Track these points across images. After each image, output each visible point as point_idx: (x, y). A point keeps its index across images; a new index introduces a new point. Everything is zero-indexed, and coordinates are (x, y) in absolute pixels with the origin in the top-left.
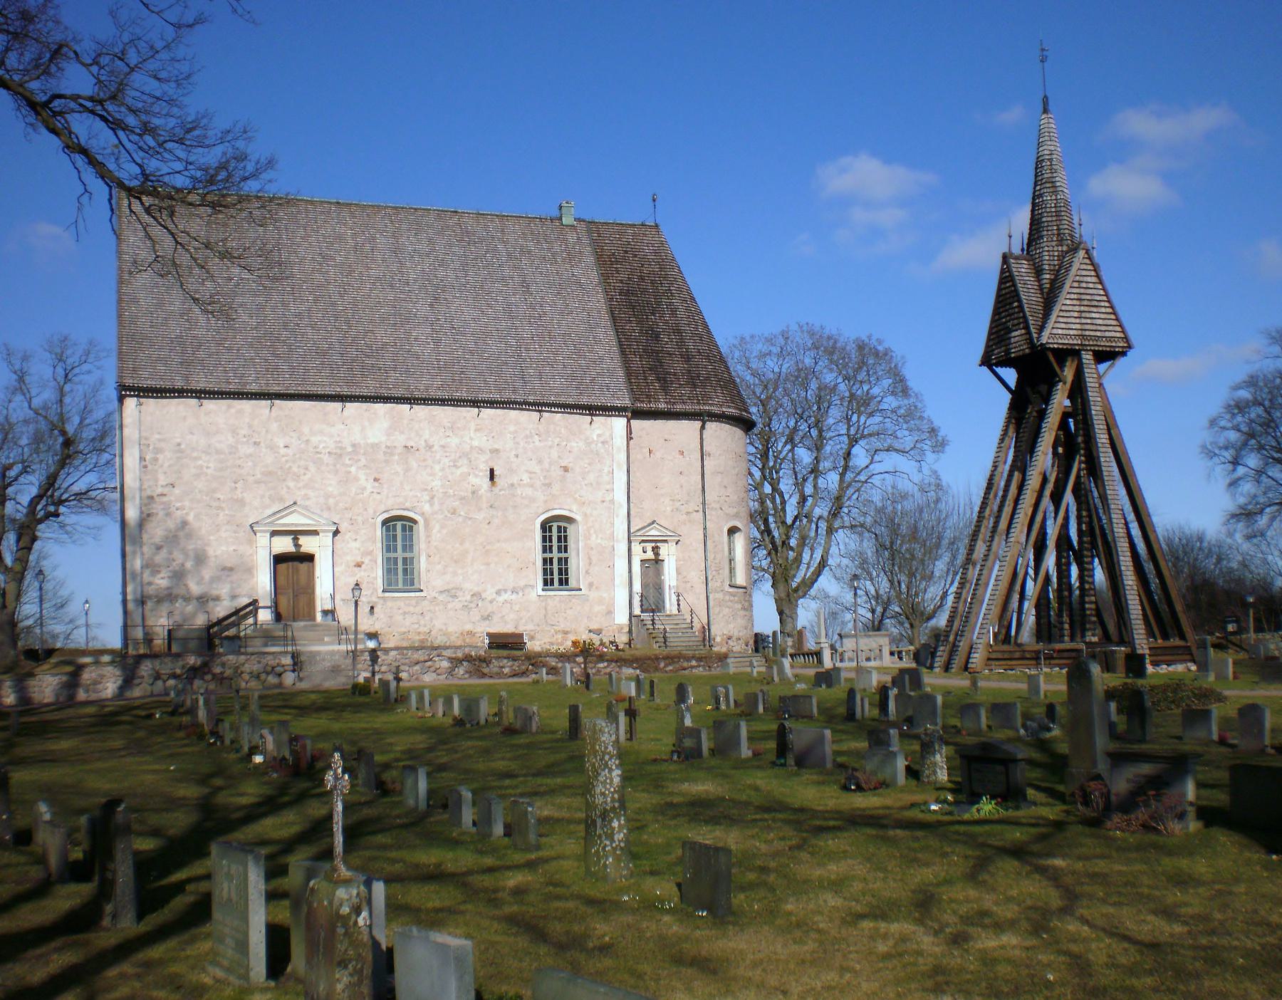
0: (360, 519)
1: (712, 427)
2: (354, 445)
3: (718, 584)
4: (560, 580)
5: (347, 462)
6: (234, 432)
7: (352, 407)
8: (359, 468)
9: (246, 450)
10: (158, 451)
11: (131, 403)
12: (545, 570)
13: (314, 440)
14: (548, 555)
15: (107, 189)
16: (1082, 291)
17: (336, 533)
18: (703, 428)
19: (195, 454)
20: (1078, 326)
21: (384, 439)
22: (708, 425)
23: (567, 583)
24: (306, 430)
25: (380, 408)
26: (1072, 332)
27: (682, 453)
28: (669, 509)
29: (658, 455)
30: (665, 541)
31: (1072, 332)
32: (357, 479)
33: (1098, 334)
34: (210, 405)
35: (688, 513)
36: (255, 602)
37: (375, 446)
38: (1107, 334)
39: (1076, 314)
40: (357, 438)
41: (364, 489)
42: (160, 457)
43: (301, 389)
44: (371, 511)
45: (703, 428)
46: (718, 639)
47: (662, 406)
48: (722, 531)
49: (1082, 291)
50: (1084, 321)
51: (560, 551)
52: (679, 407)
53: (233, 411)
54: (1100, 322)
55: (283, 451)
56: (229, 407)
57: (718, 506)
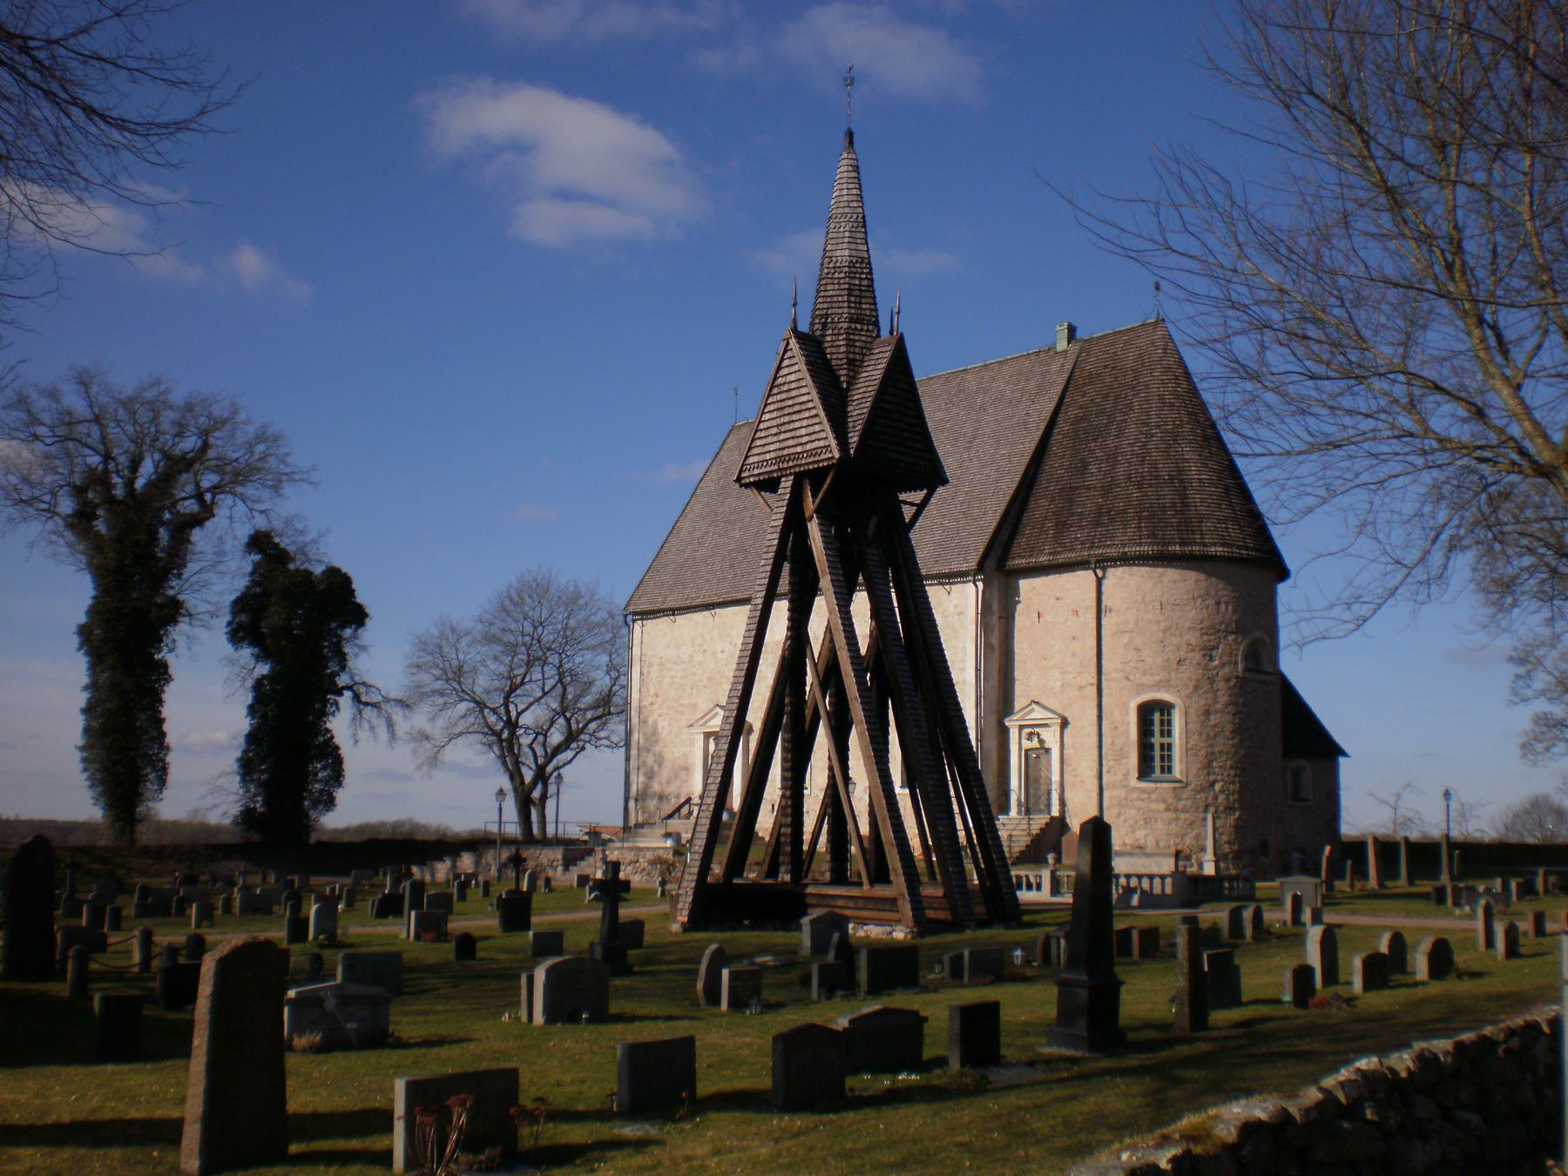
3: (1119, 777)
4: (1162, 768)
9: (699, 657)
10: (651, 665)
12: (1170, 757)
14: (1166, 740)
15: (305, 485)
16: (784, 396)
17: (1065, 723)
18: (1099, 582)
20: (777, 446)
22: (1111, 572)
23: (1170, 770)
26: (768, 456)
29: (1048, 618)
30: (1046, 725)
31: (768, 456)
33: (799, 449)
34: (682, 619)
35: (1081, 688)
36: (688, 801)
38: (808, 447)
39: (775, 430)
43: (729, 597)
45: (1099, 582)
47: (1043, 559)
49: (784, 396)
50: (782, 437)
51: (1162, 734)
52: (1061, 558)
54: (803, 431)
55: (720, 656)
57: (1121, 675)
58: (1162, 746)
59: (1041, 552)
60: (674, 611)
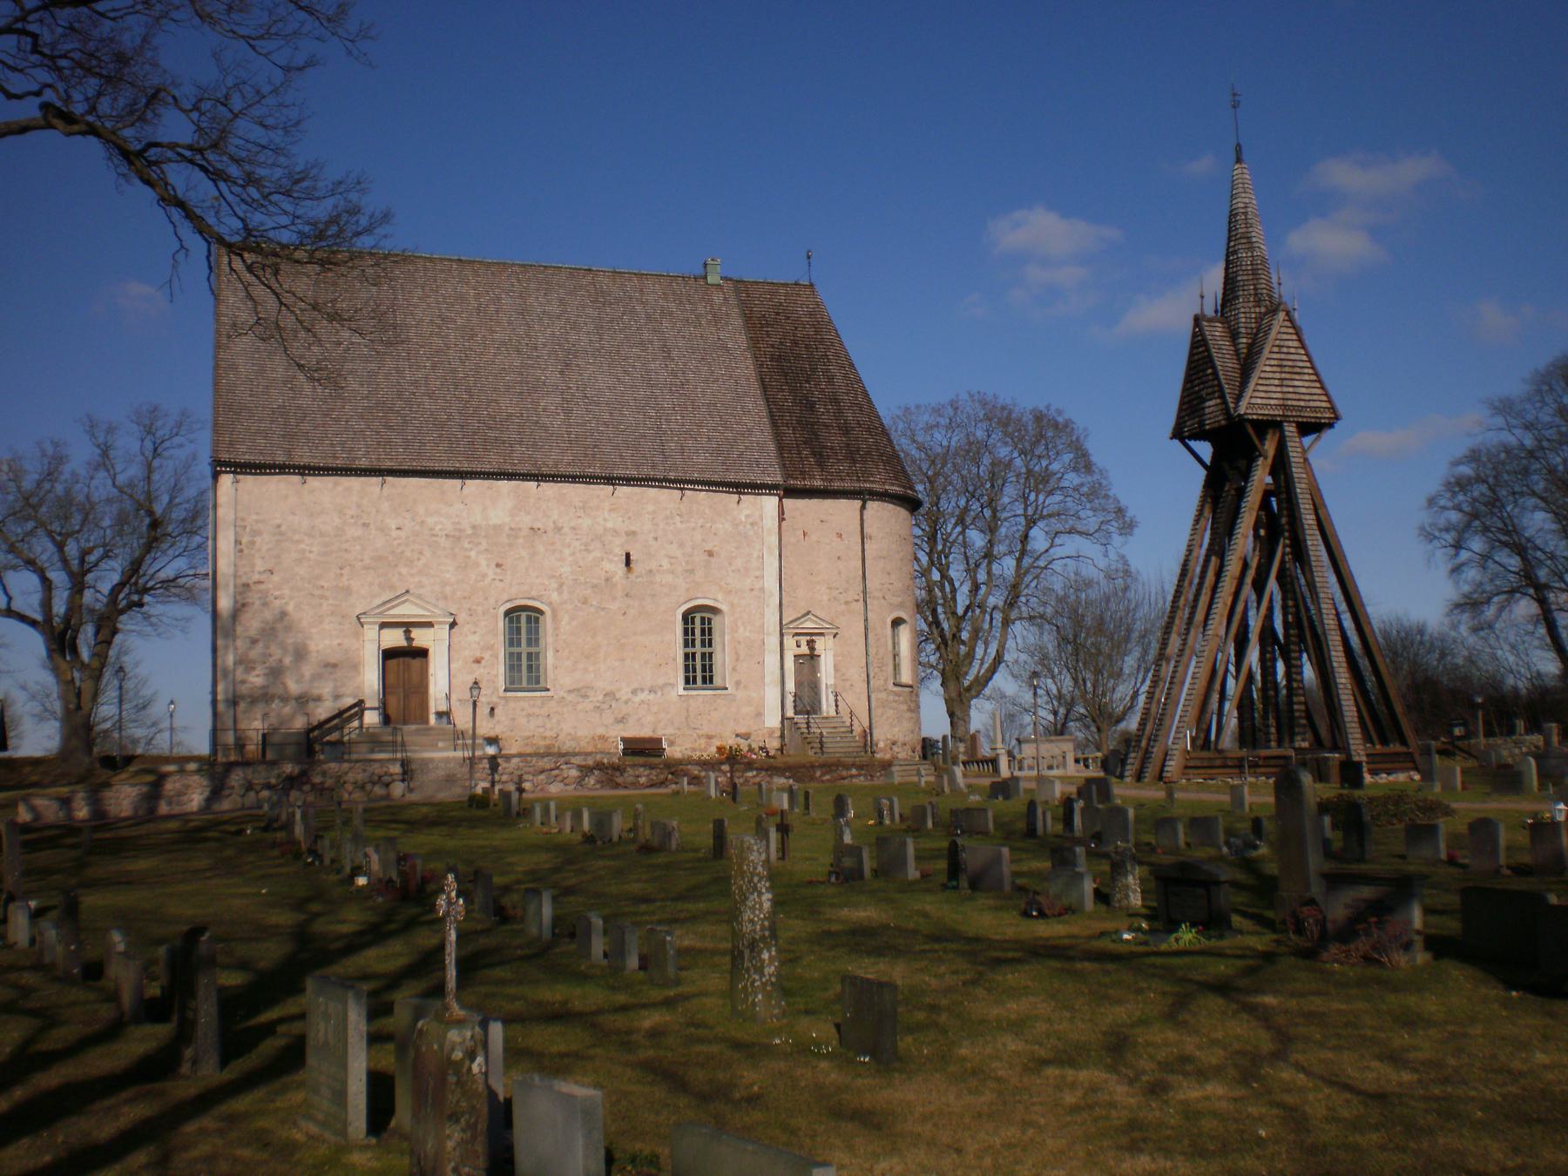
0: (480, 609)
1: (873, 506)
2: (474, 527)
5: (467, 546)
6: (341, 513)
7: (473, 485)
8: (479, 553)
11: (226, 480)
13: (430, 521)
19: (296, 537)
21: (507, 520)
22: (870, 504)
24: (421, 510)
25: (504, 485)
27: (840, 536)
28: (825, 598)
29: (814, 538)
32: (477, 565)
37: (498, 528)
40: (477, 518)
41: (484, 576)
42: (258, 540)
43: (416, 465)
44: (492, 601)
45: (863, 507)
46: (881, 745)
47: (818, 483)
48: (884, 623)
53: (340, 489)
56: (336, 484)
58: (703, 655)
59: (812, 477)
60: (305, 470)
